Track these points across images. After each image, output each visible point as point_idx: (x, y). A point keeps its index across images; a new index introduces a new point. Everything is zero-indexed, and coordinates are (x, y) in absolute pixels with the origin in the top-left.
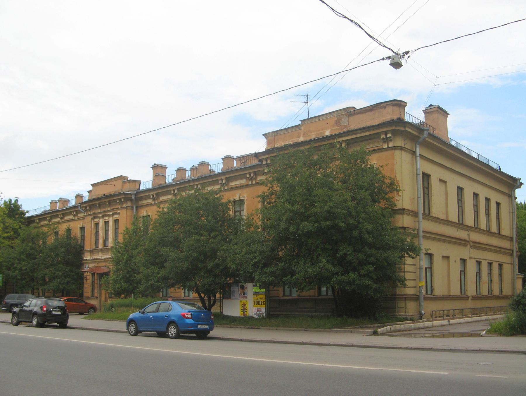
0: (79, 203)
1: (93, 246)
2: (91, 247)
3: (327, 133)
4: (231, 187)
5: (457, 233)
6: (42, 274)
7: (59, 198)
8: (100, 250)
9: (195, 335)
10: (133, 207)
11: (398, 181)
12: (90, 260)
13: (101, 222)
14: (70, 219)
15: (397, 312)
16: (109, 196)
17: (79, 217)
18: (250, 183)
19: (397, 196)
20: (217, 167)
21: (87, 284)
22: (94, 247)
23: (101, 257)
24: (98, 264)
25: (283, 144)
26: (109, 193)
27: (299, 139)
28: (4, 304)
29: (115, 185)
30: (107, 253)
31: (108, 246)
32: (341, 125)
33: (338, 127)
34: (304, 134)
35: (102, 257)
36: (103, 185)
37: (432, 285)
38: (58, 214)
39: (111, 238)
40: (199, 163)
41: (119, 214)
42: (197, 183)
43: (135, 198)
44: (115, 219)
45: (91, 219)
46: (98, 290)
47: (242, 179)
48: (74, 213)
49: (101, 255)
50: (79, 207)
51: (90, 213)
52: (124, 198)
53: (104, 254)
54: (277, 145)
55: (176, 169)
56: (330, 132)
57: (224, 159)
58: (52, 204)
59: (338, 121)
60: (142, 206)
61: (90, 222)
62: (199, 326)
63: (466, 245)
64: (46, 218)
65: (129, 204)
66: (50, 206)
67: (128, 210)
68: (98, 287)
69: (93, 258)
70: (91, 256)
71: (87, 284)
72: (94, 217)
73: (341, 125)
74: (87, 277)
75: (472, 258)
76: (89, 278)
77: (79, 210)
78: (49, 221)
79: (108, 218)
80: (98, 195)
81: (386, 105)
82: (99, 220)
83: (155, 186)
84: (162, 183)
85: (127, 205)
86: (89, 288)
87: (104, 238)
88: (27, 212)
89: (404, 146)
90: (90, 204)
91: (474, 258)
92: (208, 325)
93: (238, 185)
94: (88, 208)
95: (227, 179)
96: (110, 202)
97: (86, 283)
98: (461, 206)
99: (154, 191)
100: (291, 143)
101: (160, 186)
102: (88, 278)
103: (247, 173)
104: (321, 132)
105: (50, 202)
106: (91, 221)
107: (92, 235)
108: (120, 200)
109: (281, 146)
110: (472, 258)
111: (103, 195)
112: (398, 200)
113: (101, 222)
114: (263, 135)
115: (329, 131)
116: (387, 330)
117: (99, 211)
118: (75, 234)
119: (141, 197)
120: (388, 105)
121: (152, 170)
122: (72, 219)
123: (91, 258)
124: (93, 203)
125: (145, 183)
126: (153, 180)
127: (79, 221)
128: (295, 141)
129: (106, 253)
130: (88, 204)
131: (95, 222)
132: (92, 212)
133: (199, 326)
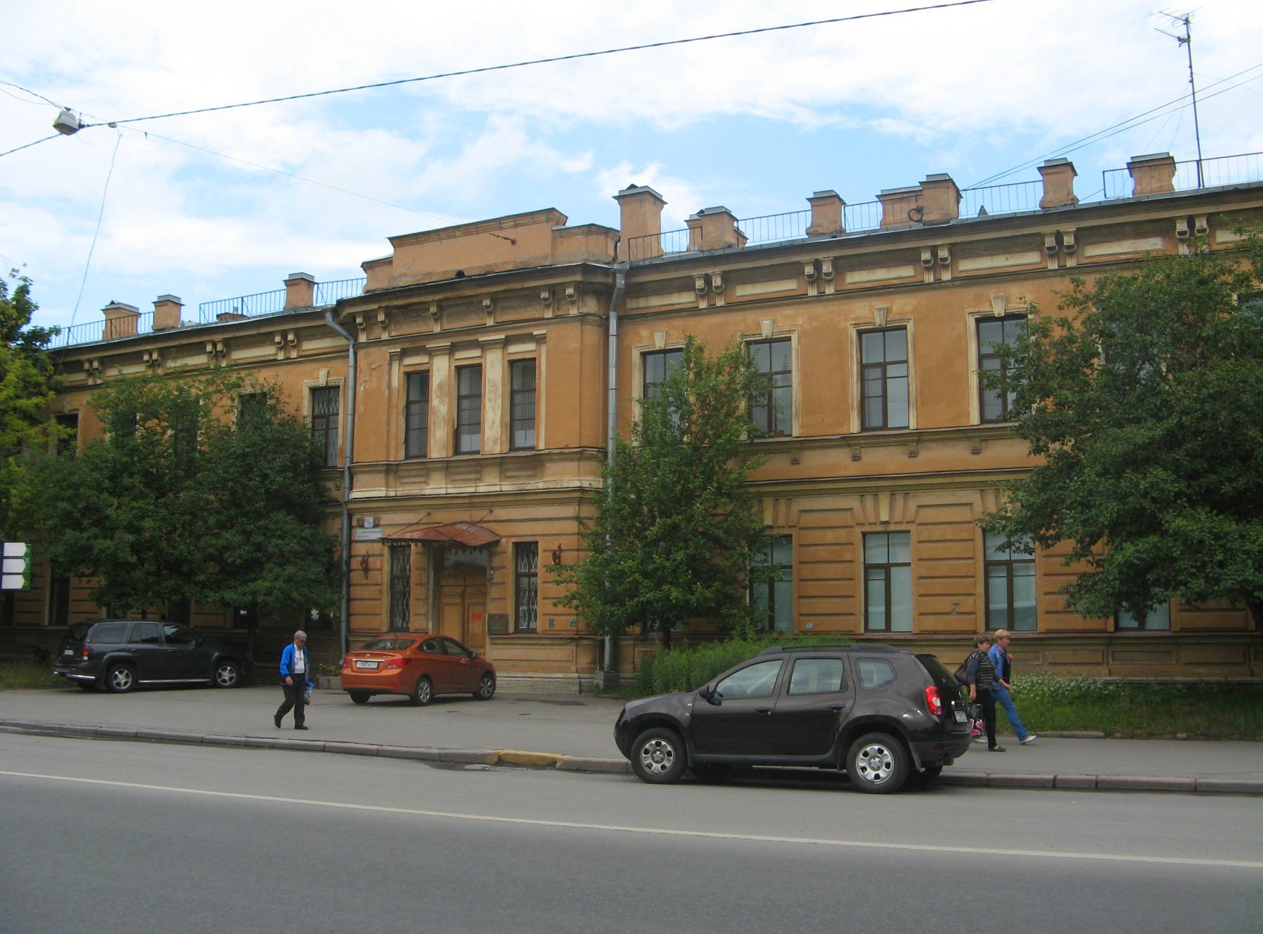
1: (397, 452)
2: (388, 455)
4: (1086, 261)
6: (212, 546)
7: (108, 303)
8: (440, 465)
10: (608, 319)
12: (387, 499)
13: (441, 370)
14: (261, 359)
16: (486, 279)
17: (304, 351)
18: (1053, 265)
20: (254, 308)
21: (368, 585)
22: (402, 456)
23: (443, 491)
24: (429, 514)
26: (488, 266)
28: (86, 658)
29: (518, 243)
30: (478, 476)
31: (781, 434)
35: (450, 491)
36: (485, 236)
38: (201, 343)
39: (493, 422)
40: (924, 179)
41: (540, 340)
42: (938, 243)
44: (512, 358)
45: (388, 356)
46: (430, 607)
47: (788, 277)
49: (444, 482)
50: (329, 316)
51: (385, 336)
52: (577, 285)
53: (456, 480)
55: (156, 300)
57: (817, 203)
58: (164, 309)
60: (644, 315)
61: (387, 367)
65: (591, 306)
66: (102, 326)
67: (587, 328)
68: (427, 594)
69: (399, 494)
70: (387, 486)
71: (368, 585)
72: (452, 343)
74: (371, 559)
76: (382, 565)
77: (326, 325)
78: (152, 365)
79: (479, 355)
80: (429, 274)
82: (482, 354)
83: (705, 248)
84: (171, 323)
85: (584, 310)
86: (380, 599)
87: (454, 426)
88: (57, 331)
93: (1123, 257)
95: (1079, 233)
96: (495, 298)
97: (365, 581)
99: (715, 265)
101: (728, 251)
102: (374, 562)
103: (277, 331)
106: (390, 364)
107: (394, 411)
108: (553, 290)
111: (453, 275)
113: (441, 370)
117: (437, 329)
118: (297, 410)
119: (642, 284)
121: (619, 206)
122: (272, 358)
123: (392, 494)
125: (202, 306)
126: (106, 320)
127: (309, 367)
129: (473, 476)
132: (394, 333)
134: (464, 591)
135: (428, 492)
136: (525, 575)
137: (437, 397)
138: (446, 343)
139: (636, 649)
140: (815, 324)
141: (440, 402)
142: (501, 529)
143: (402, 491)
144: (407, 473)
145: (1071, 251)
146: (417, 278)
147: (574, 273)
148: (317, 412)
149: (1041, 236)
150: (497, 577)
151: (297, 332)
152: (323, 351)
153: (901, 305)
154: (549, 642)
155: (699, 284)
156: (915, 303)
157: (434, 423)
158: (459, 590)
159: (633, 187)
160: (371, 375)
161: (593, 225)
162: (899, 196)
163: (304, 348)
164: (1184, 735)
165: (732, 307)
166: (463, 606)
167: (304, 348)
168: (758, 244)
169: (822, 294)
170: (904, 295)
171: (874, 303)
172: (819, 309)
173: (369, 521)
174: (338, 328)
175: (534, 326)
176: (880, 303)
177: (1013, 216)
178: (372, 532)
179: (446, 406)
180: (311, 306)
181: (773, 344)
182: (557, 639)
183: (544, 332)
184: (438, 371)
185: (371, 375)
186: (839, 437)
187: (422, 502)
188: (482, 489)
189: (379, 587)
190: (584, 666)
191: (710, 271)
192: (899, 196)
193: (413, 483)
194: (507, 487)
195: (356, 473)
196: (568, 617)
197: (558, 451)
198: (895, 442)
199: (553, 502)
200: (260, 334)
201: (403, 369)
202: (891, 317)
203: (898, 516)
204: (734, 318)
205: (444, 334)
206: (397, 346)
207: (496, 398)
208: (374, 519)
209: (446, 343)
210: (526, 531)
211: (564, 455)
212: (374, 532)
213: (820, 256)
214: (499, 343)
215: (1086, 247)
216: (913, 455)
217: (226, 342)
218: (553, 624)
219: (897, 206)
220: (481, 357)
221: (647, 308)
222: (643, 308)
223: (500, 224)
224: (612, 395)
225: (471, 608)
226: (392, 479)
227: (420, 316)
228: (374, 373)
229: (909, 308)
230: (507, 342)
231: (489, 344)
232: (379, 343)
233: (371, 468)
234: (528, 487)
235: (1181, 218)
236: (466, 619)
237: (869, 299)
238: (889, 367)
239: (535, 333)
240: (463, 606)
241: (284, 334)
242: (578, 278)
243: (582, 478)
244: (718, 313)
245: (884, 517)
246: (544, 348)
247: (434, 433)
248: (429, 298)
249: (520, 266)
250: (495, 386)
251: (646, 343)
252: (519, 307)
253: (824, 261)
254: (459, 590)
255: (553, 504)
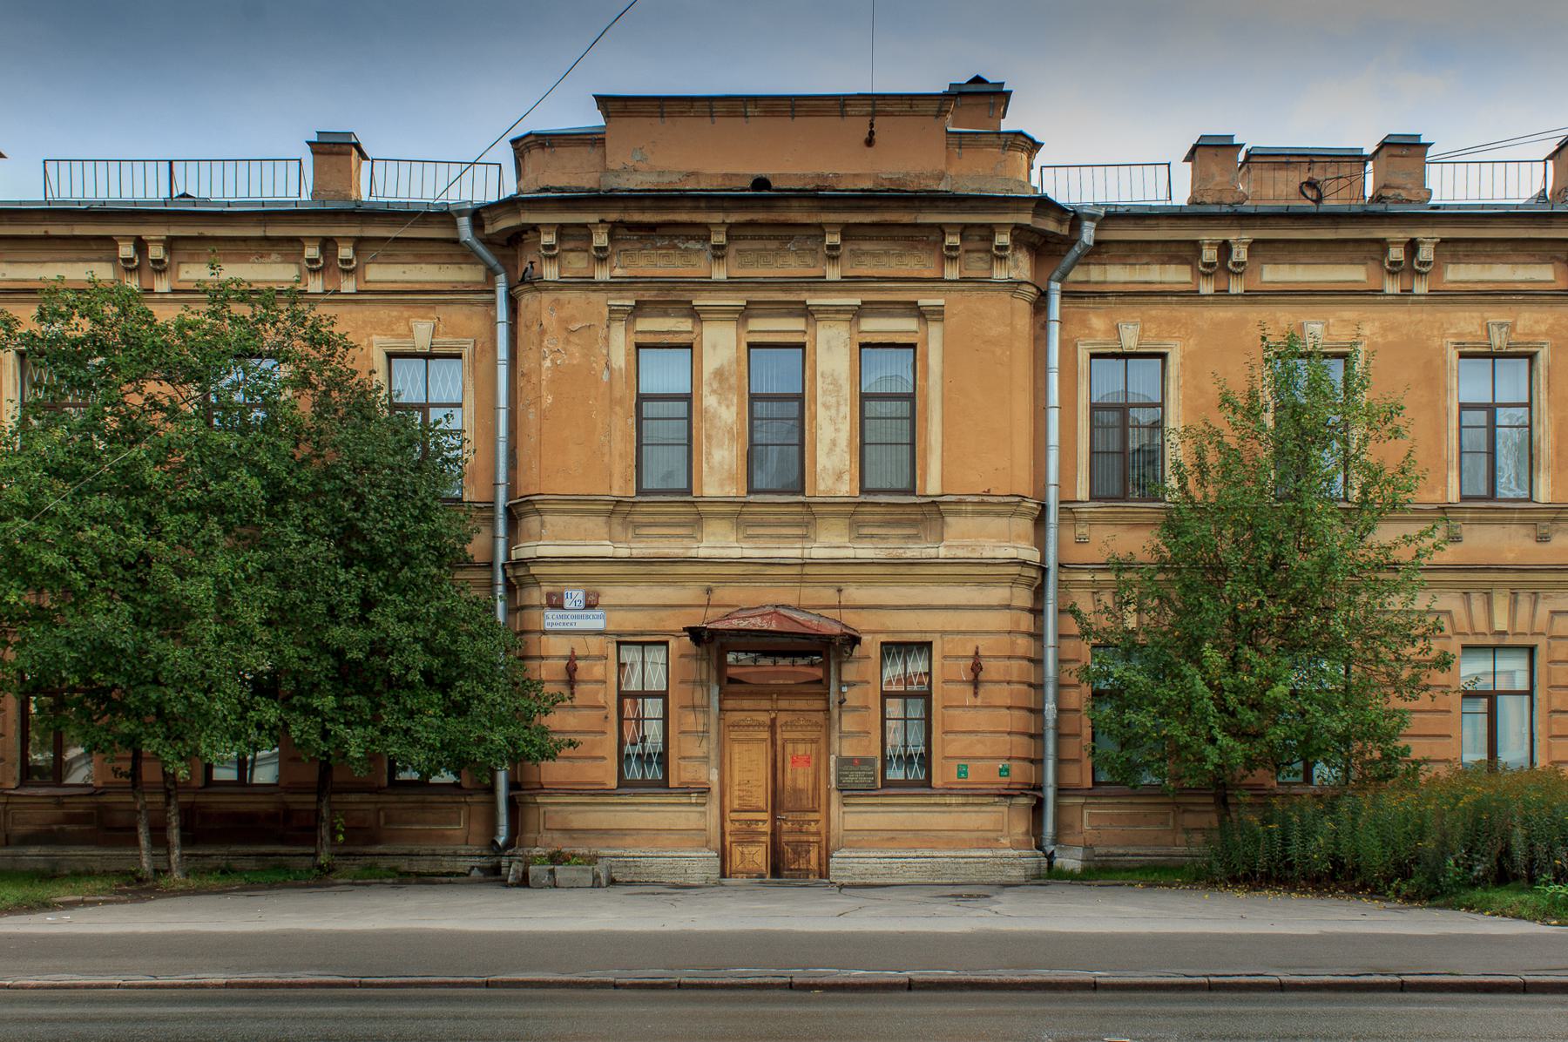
23: (735, 553)
39: (834, 443)
49: (733, 538)
50: (464, 222)
85: (1014, 274)
86: (604, 733)
111: (748, 183)
117: (719, 274)
132: (618, 272)
134: (773, 721)
135: (703, 553)
136: (635, 695)
137: (714, 392)
138: (737, 300)
139: (1085, 812)
140: (1391, 337)
141: (719, 403)
142: (855, 621)
143: (640, 549)
144: (650, 519)
145: (160, 268)
146: (666, 179)
147: (1018, 210)
148: (30, 399)
149: (1196, 245)
150: (853, 696)
151: (170, 244)
152: (417, 287)
153: (1530, 322)
154: (960, 800)
155: (1210, 254)
156: (1550, 321)
157: (709, 437)
158: (765, 718)
159: (978, 80)
160: (568, 342)
161: (1021, 134)
162: (1284, 159)
163: (183, 276)
164: (1555, 922)
165: (1251, 296)
166: (774, 743)
167: (183, 276)
168: (1282, 203)
169: (1407, 292)
170: (1535, 308)
171: (1486, 315)
172: (1399, 315)
173: (574, 597)
174: (480, 248)
175: (920, 289)
176: (1495, 315)
177: (1177, 210)
178: (582, 617)
179: (734, 409)
180: (347, 198)
181: (1497, 360)
182: (973, 794)
183: (941, 302)
184: (714, 347)
185: (568, 342)
186: (1435, 506)
187: (935, 570)
188: (818, 553)
189: (603, 712)
190: (1021, 838)
191: (1232, 236)
192: (1284, 159)
193: (662, 536)
194: (866, 551)
195: (522, 515)
196: (992, 763)
197: (976, 499)
198: (1520, 519)
199: (962, 580)
200: (266, 239)
201: (634, 339)
202: (1514, 338)
203: (1522, 623)
204: (1255, 314)
205: (733, 284)
206: (625, 294)
207: (838, 404)
208: (587, 595)
209: (737, 300)
210: (908, 625)
211: (986, 505)
212: (588, 617)
213: (1419, 234)
214: (846, 312)
215: (367, 266)
216: (1543, 539)
217: (170, 244)
218: (966, 773)
219: (1281, 175)
220: (805, 332)
221: (1104, 282)
222: (1097, 283)
223: (845, 105)
224: (1054, 416)
225: (789, 748)
226: (618, 530)
227: (675, 247)
228: (573, 338)
229: (1543, 327)
230: (859, 312)
231: (827, 312)
232: (588, 284)
233: (581, 505)
234: (909, 554)
235: (126, 238)
236: (779, 765)
237: (1481, 308)
238: (1500, 411)
239: (921, 302)
240: (774, 743)
241: (327, 244)
242: (1026, 219)
243: (632, 545)
244: (1232, 303)
245: (1501, 623)
246: (935, 330)
247: (709, 453)
248: (717, 217)
249: (887, 185)
250: (835, 382)
251: (1100, 338)
252: (886, 253)
253: (1422, 242)
254: (765, 718)
255: (940, 583)
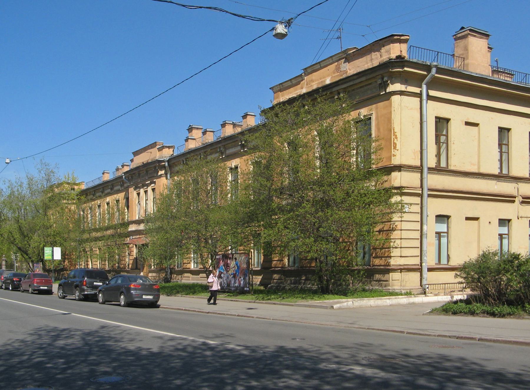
0: (123, 173)
3: (328, 82)
5: (496, 187)
9: (37, 292)
11: (396, 133)
15: (390, 285)
19: (394, 150)
25: (288, 98)
27: (302, 91)
32: (341, 71)
33: (338, 74)
34: (307, 85)
37: (449, 253)
43: (168, 164)
48: (120, 183)
54: (282, 99)
56: (330, 80)
59: (338, 66)
62: (144, 297)
63: (513, 202)
64: (108, 186)
73: (341, 71)
75: (521, 217)
81: (385, 42)
89: (406, 90)
90: (132, 173)
91: (527, 217)
92: (47, 287)
94: (130, 178)
98: (507, 152)
100: (295, 95)
104: (322, 81)
105: (185, 140)
109: (286, 100)
110: (521, 217)
112: (395, 156)
114: (270, 89)
115: (330, 78)
116: (348, 305)
120: (387, 41)
124: (134, 172)
128: (298, 94)
130: (130, 174)
131: (137, 192)
133: (144, 297)
